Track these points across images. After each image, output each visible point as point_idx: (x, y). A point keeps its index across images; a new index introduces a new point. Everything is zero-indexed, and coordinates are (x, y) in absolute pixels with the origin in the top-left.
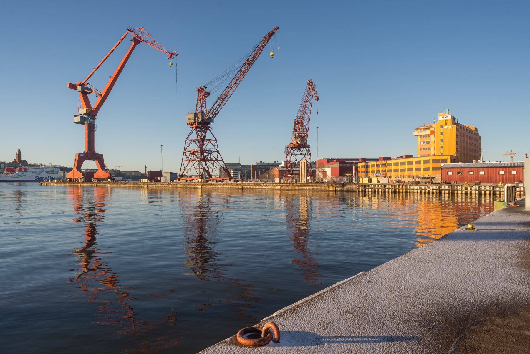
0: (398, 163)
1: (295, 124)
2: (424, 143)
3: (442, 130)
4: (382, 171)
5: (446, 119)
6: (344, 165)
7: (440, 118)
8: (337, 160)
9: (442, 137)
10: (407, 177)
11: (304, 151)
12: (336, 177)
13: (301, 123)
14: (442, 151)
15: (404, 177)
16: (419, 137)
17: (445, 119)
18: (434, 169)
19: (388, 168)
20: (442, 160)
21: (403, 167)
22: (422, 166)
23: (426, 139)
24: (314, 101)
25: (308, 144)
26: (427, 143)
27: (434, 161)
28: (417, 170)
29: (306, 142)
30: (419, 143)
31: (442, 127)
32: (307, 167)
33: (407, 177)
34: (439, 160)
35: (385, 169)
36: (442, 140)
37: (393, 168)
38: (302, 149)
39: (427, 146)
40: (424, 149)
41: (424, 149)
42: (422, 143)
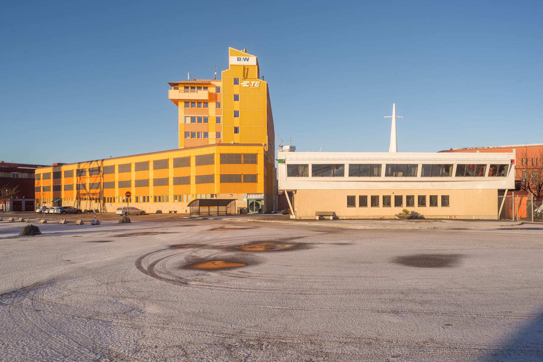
0: (129, 165)
2: (193, 119)
3: (236, 90)
4: (92, 186)
7: (233, 60)
9: (236, 105)
10: (152, 199)
14: (237, 138)
15: (146, 199)
16: (181, 105)
17: (243, 63)
18: (225, 179)
19: (107, 178)
20: (246, 156)
22: (193, 171)
23: (198, 112)
26: (200, 120)
27: (226, 159)
28: (178, 181)
30: (181, 120)
31: (236, 82)
32: (131, 200)
33: (152, 199)
35: (98, 181)
36: (236, 114)
37: (117, 177)
41: (193, 135)
42: (189, 120)
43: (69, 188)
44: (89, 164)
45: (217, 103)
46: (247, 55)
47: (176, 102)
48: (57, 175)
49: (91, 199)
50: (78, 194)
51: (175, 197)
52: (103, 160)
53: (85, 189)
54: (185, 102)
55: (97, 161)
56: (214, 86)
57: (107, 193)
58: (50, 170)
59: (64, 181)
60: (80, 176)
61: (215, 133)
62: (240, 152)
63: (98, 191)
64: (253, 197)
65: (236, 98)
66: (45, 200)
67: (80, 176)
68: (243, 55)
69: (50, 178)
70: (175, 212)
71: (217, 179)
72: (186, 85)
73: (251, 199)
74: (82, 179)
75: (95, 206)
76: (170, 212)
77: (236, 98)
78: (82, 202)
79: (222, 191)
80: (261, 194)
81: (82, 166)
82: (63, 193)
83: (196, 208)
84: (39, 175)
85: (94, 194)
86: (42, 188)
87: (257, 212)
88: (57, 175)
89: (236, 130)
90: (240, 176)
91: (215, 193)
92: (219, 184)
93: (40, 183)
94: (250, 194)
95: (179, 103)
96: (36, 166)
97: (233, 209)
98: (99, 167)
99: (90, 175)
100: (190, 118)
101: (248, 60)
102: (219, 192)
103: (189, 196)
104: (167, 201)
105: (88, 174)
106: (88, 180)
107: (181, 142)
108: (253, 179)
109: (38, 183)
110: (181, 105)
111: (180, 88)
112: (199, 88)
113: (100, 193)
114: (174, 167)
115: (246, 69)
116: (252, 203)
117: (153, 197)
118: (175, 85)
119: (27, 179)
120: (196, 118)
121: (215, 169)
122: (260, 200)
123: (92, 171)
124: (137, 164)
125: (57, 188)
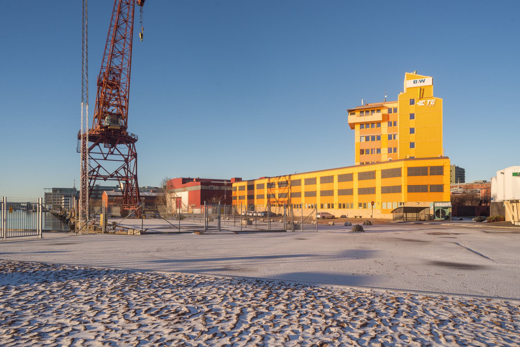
2: (367, 139)
3: (412, 109)
4: (281, 195)
5: (422, 84)
6: (209, 187)
7: (408, 83)
8: (198, 180)
9: (412, 123)
10: (336, 206)
11: (123, 148)
13: (114, 85)
14: (412, 152)
16: (357, 127)
17: (419, 84)
18: (411, 189)
19: (295, 189)
20: (432, 168)
23: (371, 132)
25: (130, 131)
26: (373, 138)
27: (413, 172)
28: (324, 193)
29: (125, 128)
30: (357, 140)
31: (412, 102)
33: (336, 206)
34: (426, 168)
35: (286, 191)
37: (303, 188)
39: (371, 145)
42: (364, 139)
43: (261, 197)
45: (388, 122)
46: (423, 77)
47: (352, 126)
48: (251, 187)
49: (279, 206)
50: (269, 201)
51: (360, 205)
52: (290, 175)
53: (275, 197)
54: (361, 124)
55: (285, 176)
56: (386, 108)
57: (295, 201)
58: (245, 184)
59: (256, 192)
60: (270, 188)
63: (286, 199)
64: (439, 205)
66: (241, 207)
67: (270, 188)
68: (419, 78)
69: (244, 190)
70: (361, 217)
71: (404, 189)
72: (362, 110)
73: (437, 207)
74: (272, 191)
75: (282, 210)
76: (355, 217)
77: (412, 116)
78: (272, 208)
79: (409, 200)
80: (448, 202)
81: (272, 181)
83: (401, 214)
85: (282, 202)
86: (238, 197)
87: (443, 219)
88: (251, 187)
89: (412, 145)
90: (426, 186)
91: (403, 201)
93: (237, 193)
94: (436, 202)
96: (254, 180)
97: (422, 215)
98: (287, 181)
99: (280, 187)
101: (424, 82)
102: (406, 200)
104: (352, 207)
105: (277, 186)
106: (277, 191)
107: (357, 159)
108: (439, 188)
109: (235, 194)
110: (357, 127)
112: (373, 111)
113: (288, 201)
114: (359, 180)
115: (422, 90)
116: (438, 211)
117: (337, 204)
118: (352, 112)
120: (370, 138)
121: (403, 181)
122: (447, 208)
124: (306, 180)
125: (251, 197)
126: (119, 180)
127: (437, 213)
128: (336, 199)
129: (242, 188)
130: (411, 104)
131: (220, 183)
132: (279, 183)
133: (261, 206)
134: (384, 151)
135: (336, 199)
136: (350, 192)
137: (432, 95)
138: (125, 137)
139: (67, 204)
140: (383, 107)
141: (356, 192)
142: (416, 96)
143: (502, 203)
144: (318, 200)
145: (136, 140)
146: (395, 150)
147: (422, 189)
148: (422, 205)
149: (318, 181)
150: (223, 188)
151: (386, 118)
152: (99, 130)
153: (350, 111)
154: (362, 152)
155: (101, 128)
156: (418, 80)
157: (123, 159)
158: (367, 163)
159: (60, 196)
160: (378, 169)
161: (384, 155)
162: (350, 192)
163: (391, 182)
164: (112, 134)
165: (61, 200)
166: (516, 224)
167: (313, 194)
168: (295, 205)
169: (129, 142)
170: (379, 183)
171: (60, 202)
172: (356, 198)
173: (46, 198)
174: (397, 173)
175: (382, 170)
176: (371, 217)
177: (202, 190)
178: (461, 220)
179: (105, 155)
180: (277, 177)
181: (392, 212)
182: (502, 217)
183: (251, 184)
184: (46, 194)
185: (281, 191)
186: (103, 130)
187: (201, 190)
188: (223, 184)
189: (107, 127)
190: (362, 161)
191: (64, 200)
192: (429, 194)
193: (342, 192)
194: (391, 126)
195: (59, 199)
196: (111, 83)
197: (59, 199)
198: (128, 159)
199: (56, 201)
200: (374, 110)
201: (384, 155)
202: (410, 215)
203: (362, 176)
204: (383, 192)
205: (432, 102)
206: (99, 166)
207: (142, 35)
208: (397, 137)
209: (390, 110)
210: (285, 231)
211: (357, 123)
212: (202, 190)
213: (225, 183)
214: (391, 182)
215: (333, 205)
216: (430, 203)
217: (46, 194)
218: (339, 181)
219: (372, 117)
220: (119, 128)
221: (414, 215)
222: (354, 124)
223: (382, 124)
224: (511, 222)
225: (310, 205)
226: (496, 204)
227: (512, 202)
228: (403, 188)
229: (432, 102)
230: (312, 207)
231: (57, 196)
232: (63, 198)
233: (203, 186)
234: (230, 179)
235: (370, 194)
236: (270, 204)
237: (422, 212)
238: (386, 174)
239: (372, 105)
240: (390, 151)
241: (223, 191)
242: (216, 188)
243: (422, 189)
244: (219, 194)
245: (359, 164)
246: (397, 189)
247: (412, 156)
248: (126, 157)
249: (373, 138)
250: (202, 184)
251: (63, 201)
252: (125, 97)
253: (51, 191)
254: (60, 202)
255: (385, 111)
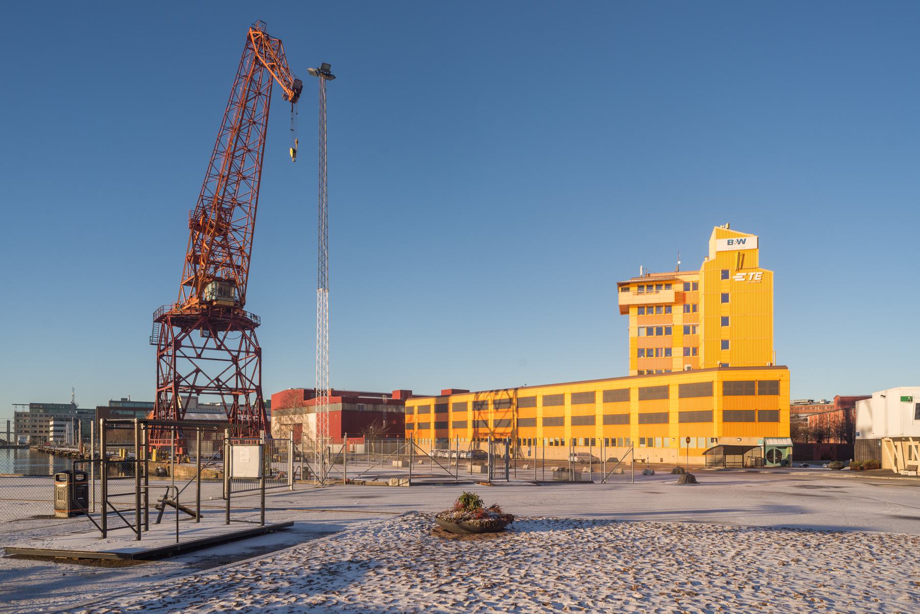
1: (196, 226)
2: (650, 331)
3: (725, 286)
4: (498, 424)
5: (741, 247)
6: (356, 407)
7: (717, 244)
8: (334, 393)
11: (233, 339)
12: (333, 441)
13: (222, 228)
14: (725, 357)
16: (633, 312)
17: (736, 247)
18: (730, 416)
19: (524, 413)
20: (762, 384)
21: (41, 429)
23: (655, 319)
24: (280, 107)
25: (249, 309)
26: (659, 331)
27: (731, 389)
28: (577, 421)
29: (241, 303)
30: (633, 333)
31: (725, 274)
35: (509, 416)
38: (221, 335)
40: (650, 353)
43: (462, 425)
44: (493, 394)
46: (742, 235)
47: (625, 310)
48: (442, 408)
50: (476, 434)
52: (516, 389)
53: (487, 426)
55: (506, 390)
58: (431, 402)
59: (453, 416)
60: (479, 410)
61: (682, 349)
62: (752, 378)
63: (509, 430)
65: (725, 298)
66: (426, 443)
67: (479, 410)
68: (735, 236)
70: (643, 461)
71: (717, 416)
77: (725, 298)
79: (726, 433)
81: (482, 397)
82: (451, 432)
83: (720, 457)
84: (413, 408)
85: (502, 434)
87: (779, 464)
88: (442, 408)
89: (725, 345)
92: (721, 424)
93: (416, 418)
95: (631, 310)
100: (645, 330)
103: (666, 439)
105: (491, 407)
106: (491, 415)
110: (633, 312)
111: (631, 289)
112: (659, 286)
113: (512, 433)
114: (640, 399)
115: (741, 256)
118: (624, 287)
119: (753, 436)
122: (785, 447)
123: (500, 403)
125: (442, 426)
126: (222, 394)
127: (769, 455)
128: (599, 431)
129: (424, 410)
130: (723, 278)
131: (375, 399)
132: (495, 402)
133: (461, 441)
134: (677, 352)
135: (599, 431)
136: (624, 419)
137: (757, 265)
138: (241, 320)
139: (62, 434)
140: (676, 281)
141: (634, 419)
142: (732, 266)
143: (878, 441)
144: (567, 432)
145: (257, 325)
146: (695, 351)
147: (745, 416)
148: (745, 442)
149: (568, 400)
150: (380, 408)
151: (680, 298)
152: (197, 306)
153: (620, 285)
154: (640, 352)
155: (201, 303)
156: (735, 240)
157: (230, 358)
158: (650, 373)
159: (44, 418)
160: (673, 383)
161: (678, 361)
162: (624, 419)
163: (696, 404)
164: (222, 316)
165: (49, 426)
166: (902, 473)
167: (558, 422)
168: (525, 440)
169: (243, 329)
170: (674, 405)
171: (44, 429)
172: (634, 430)
173: (17, 421)
174: (705, 390)
175: (680, 385)
176: (662, 460)
177: (344, 412)
178: (806, 466)
179: (199, 351)
180: (491, 391)
181: (705, 454)
182: (876, 462)
183: (442, 402)
184: (18, 415)
185: (500, 416)
186: (205, 307)
187: (343, 411)
188: (381, 402)
189: (212, 301)
190: (641, 369)
191: (54, 425)
192: (757, 425)
193: (609, 420)
194: (688, 311)
195: (44, 424)
196: (212, 225)
197: (44, 424)
198: (238, 357)
199: (38, 429)
200: (661, 285)
201: (678, 361)
202: (730, 459)
203: (646, 394)
204: (681, 421)
205: (757, 276)
206: (198, 371)
207: (294, 152)
208: (700, 331)
209: (687, 286)
210: (592, 482)
211: (634, 306)
212: (343, 411)
213: (385, 398)
214: (696, 404)
215: (535, 440)
216: (755, 437)
217: (18, 415)
218: (605, 400)
219: (657, 296)
220: (232, 304)
221: (738, 458)
222: (628, 306)
223: (673, 308)
224: (891, 471)
225: (552, 440)
226: (867, 442)
227: (895, 439)
228: (715, 414)
229: (757, 276)
230: (557, 444)
231: (38, 418)
232: (51, 423)
233: (346, 404)
234: (390, 392)
235: (652, 423)
236: (477, 439)
237: (748, 453)
238: (686, 391)
239: (656, 275)
240: (686, 352)
241: (382, 412)
242: (369, 408)
243: (745, 416)
244: (376, 417)
245: (636, 373)
246: (705, 417)
247: (724, 361)
248: (235, 354)
249: (659, 331)
250: (344, 401)
251: (51, 428)
252: (241, 250)
253: (27, 409)
254: (44, 429)
255: (679, 287)
